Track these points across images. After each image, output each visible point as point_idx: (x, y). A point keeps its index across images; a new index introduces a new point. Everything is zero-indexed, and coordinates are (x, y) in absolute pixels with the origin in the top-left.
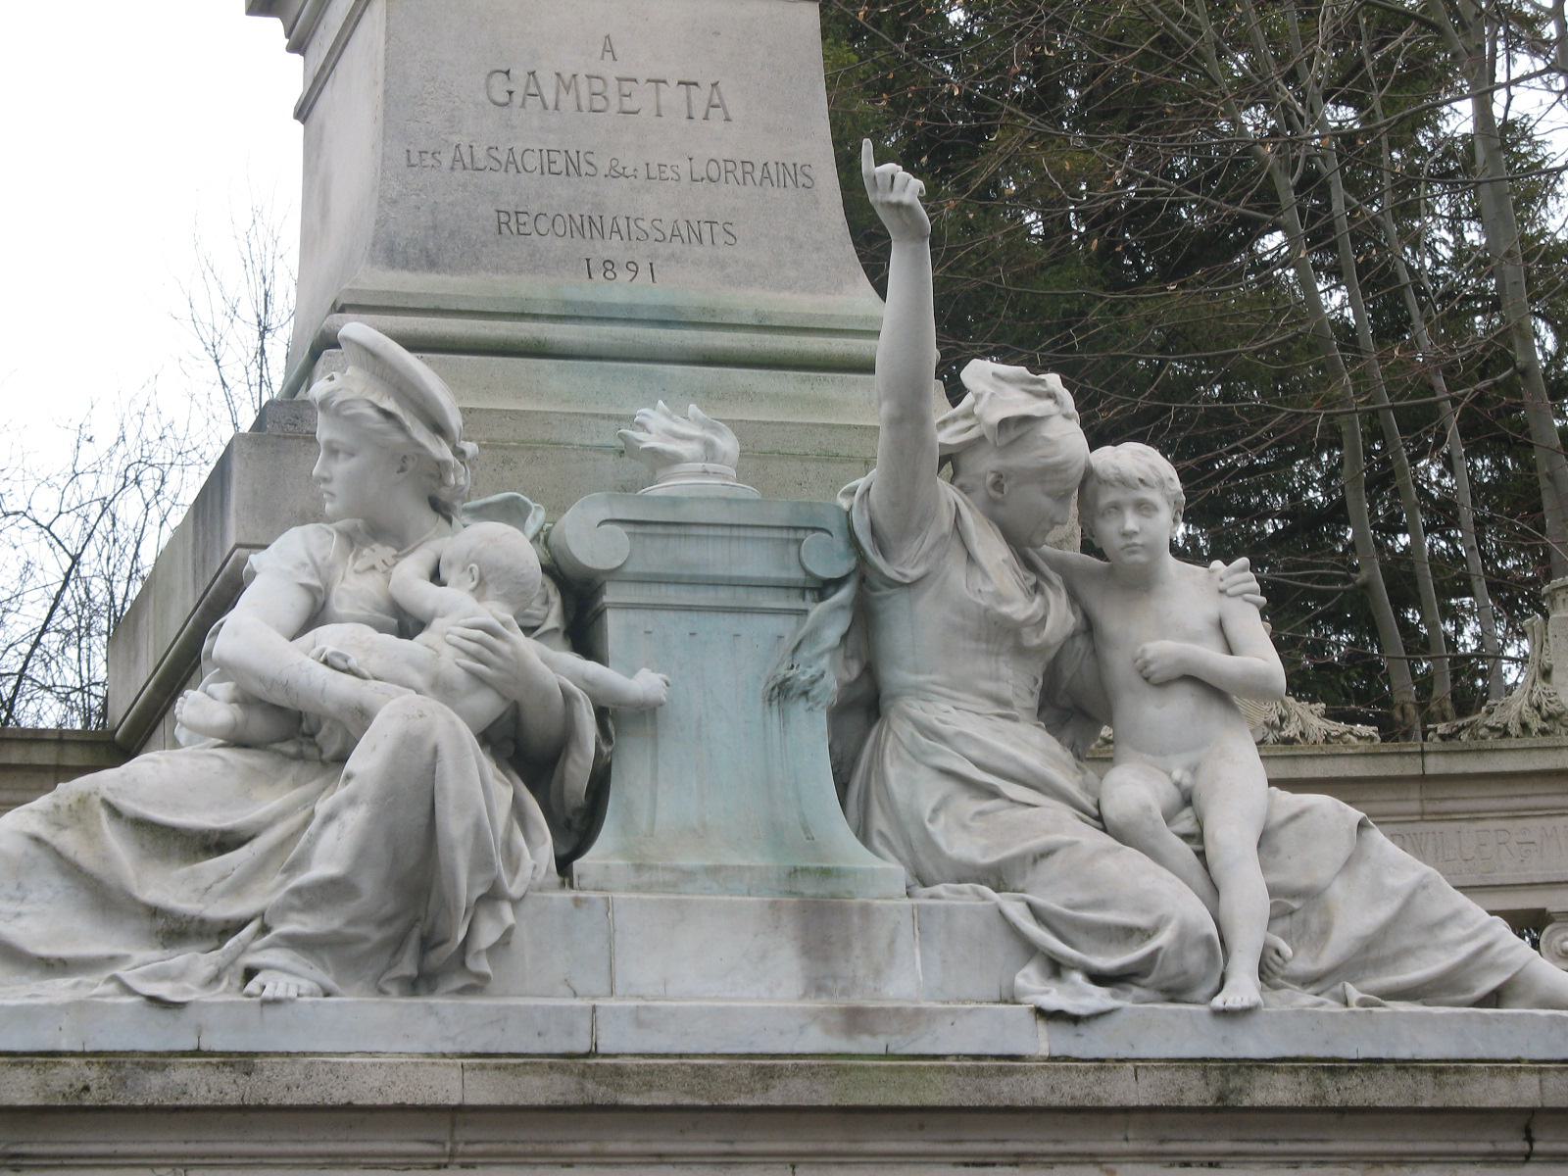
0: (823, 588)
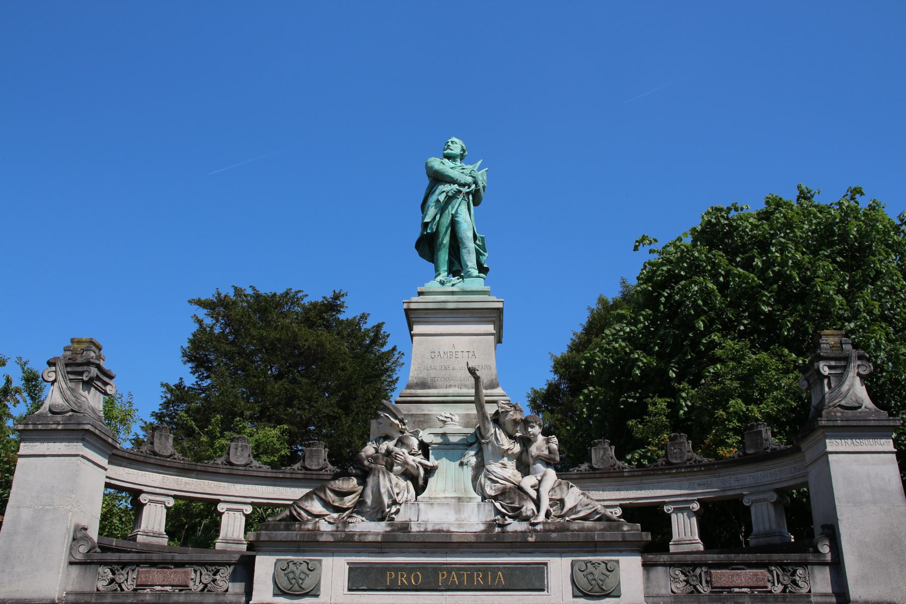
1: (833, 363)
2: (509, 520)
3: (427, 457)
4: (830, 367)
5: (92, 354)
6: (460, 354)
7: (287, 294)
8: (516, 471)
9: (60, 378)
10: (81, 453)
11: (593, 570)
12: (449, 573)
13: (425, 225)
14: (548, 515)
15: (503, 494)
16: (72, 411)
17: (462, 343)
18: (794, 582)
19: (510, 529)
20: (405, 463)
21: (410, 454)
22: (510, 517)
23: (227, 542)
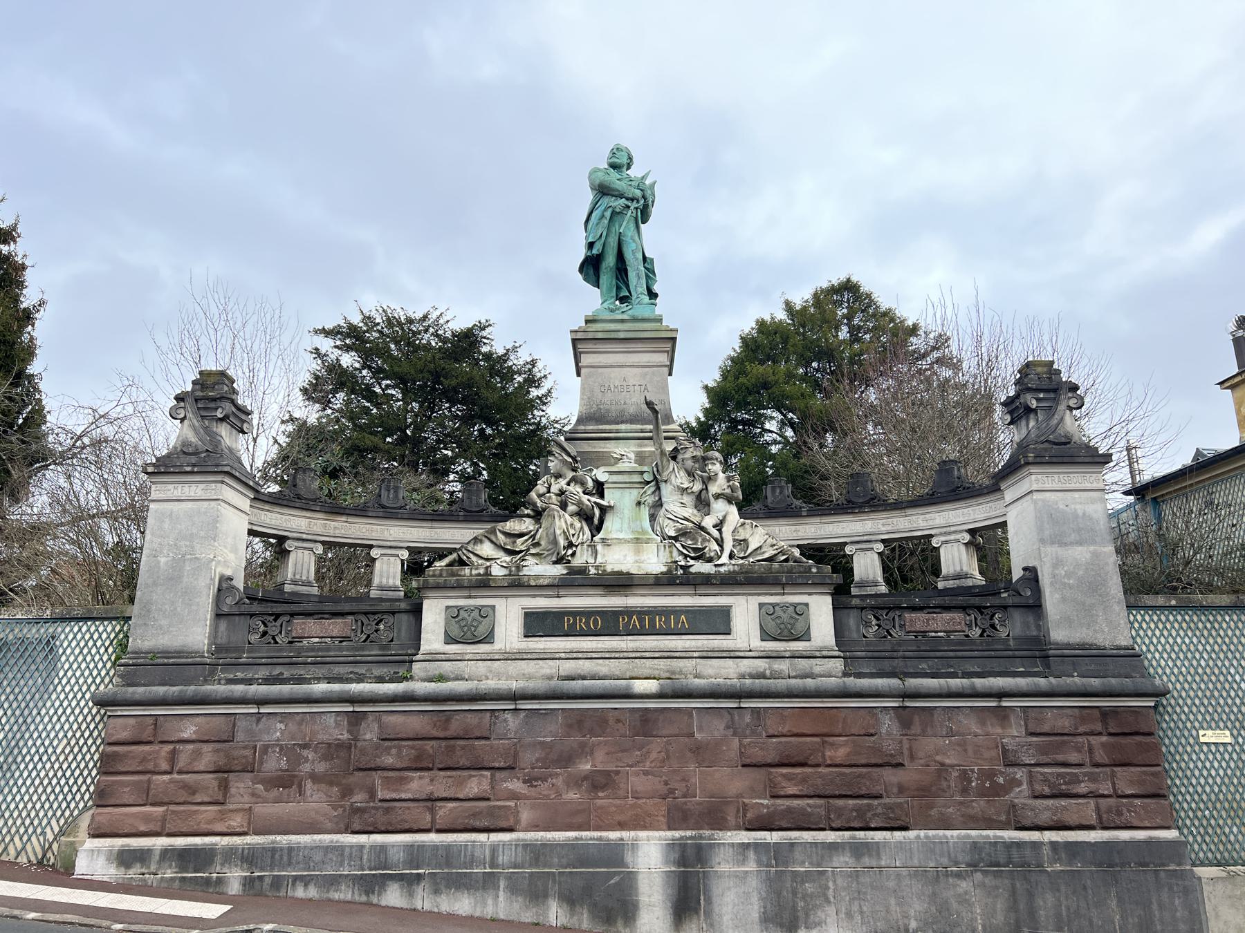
0: (648, 483)
1: (1041, 396)
2: (692, 562)
3: (602, 496)
4: (1038, 400)
5: (226, 388)
6: (631, 388)
7: (425, 317)
8: (695, 512)
9: (190, 415)
11: (781, 613)
12: (630, 618)
13: (591, 245)
14: (731, 556)
15: (682, 534)
17: (633, 376)
18: (993, 626)
19: (692, 570)
20: (580, 503)
21: (584, 493)
22: (692, 558)
23: (381, 588)
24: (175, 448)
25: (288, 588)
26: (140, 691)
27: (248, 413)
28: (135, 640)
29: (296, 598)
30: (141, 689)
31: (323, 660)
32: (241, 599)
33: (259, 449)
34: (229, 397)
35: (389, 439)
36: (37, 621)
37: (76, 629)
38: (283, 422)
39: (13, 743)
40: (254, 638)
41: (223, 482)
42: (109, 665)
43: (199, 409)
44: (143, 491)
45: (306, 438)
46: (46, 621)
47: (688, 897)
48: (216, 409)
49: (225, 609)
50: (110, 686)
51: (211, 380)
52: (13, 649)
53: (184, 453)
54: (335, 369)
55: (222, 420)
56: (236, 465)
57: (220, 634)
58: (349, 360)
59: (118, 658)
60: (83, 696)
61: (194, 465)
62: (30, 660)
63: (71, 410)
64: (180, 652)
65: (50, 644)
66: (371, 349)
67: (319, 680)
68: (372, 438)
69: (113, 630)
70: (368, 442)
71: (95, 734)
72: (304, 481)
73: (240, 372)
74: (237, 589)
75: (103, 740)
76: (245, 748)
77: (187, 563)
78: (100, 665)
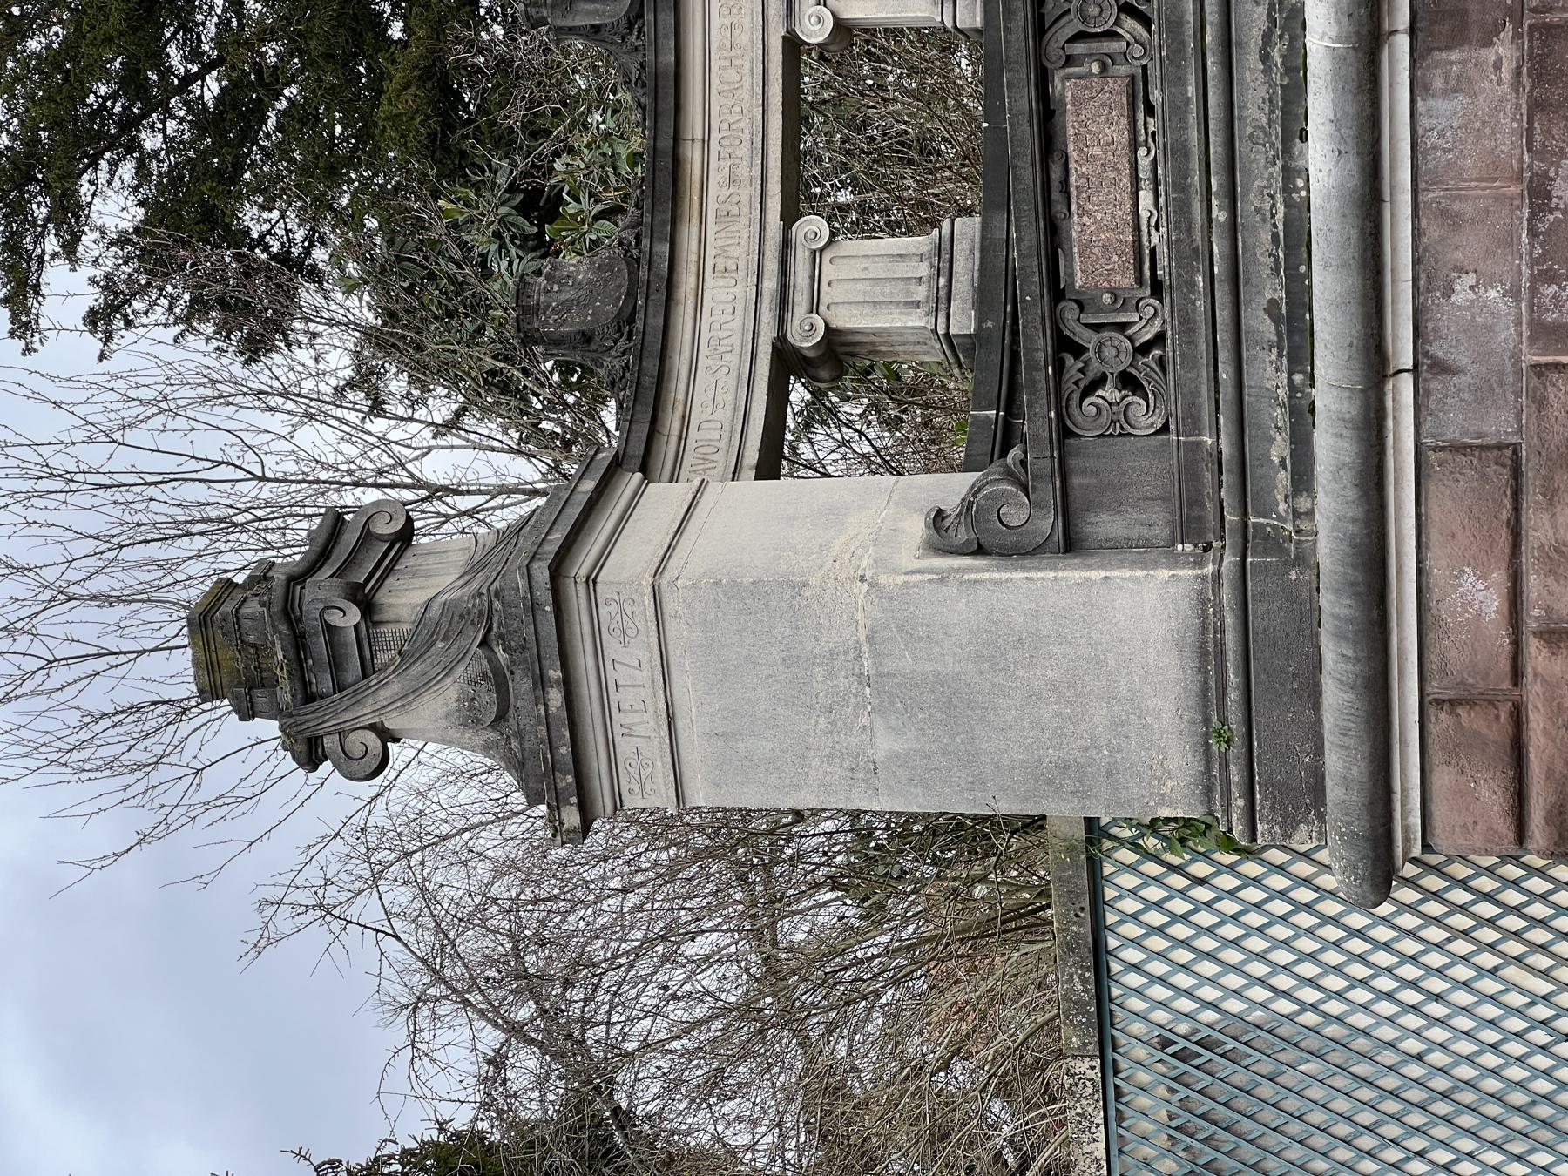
5: (253, 607)
9: (365, 712)
10: (647, 581)
16: (484, 643)
24: (487, 748)
25: (963, 321)
26: (1341, 764)
27: (336, 521)
28: (1163, 800)
29: (996, 293)
30: (1333, 761)
31: (1214, 167)
32: (1009, 475)
33: (469, 470)
34: (283, 592)
35: (396, 31)
36: (1111, 1094)
37: (1134, 980)
38: (377, 408)
39: (1518, 1122)
40: (1144, 417)
41: (591, 581)
42: (1252, 868)
43: (339, 687)
44: (658, 828)
45: (430, 325)
46: (1109, 1068)
47: (1564, 9)
48: (330, 629)
49: (1047, 523)
50: (1323, 856)
51: (228, 656)
52: (1208, 1154)
53: (501, 716)
54: (157, 249)
55: (369, 609)
56: (526, 543)
57: (1138, 532)
58: (113, 204)
59: (1228, 844)
60: (1360, 933)
61: (541, 682)
62: (1242, 1102)
63: (425, 1067)
64: (1203, 654)
65: (1184, 1052)
66: (55, 124)
67: (1292, 174)
68: (391, 87)
69: (1132, 868)
70: (408, 102)
71: (1486, 884)
72: (566, 307)
73: (194, 568)
74: (975, 491)
75: (1505, 859)
76: (1541, 403)
77: (891, 665)
78: (1253, 894)
